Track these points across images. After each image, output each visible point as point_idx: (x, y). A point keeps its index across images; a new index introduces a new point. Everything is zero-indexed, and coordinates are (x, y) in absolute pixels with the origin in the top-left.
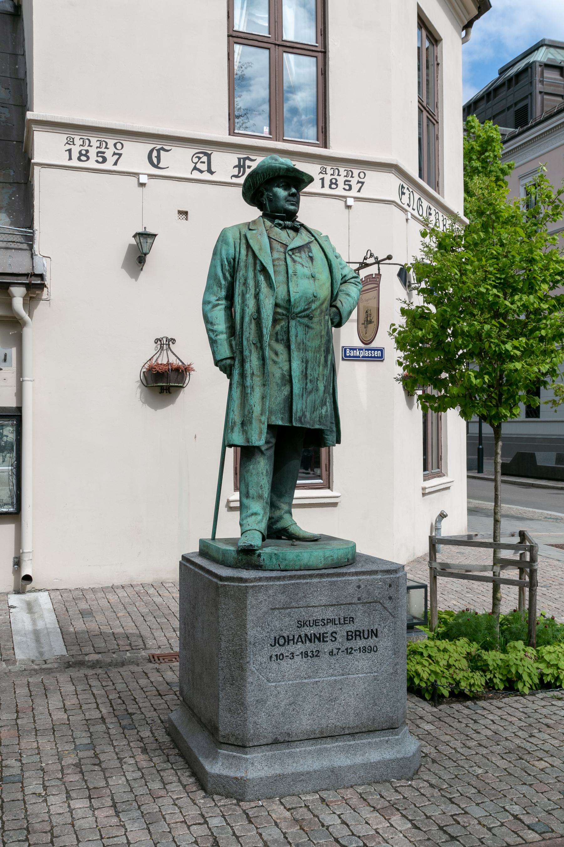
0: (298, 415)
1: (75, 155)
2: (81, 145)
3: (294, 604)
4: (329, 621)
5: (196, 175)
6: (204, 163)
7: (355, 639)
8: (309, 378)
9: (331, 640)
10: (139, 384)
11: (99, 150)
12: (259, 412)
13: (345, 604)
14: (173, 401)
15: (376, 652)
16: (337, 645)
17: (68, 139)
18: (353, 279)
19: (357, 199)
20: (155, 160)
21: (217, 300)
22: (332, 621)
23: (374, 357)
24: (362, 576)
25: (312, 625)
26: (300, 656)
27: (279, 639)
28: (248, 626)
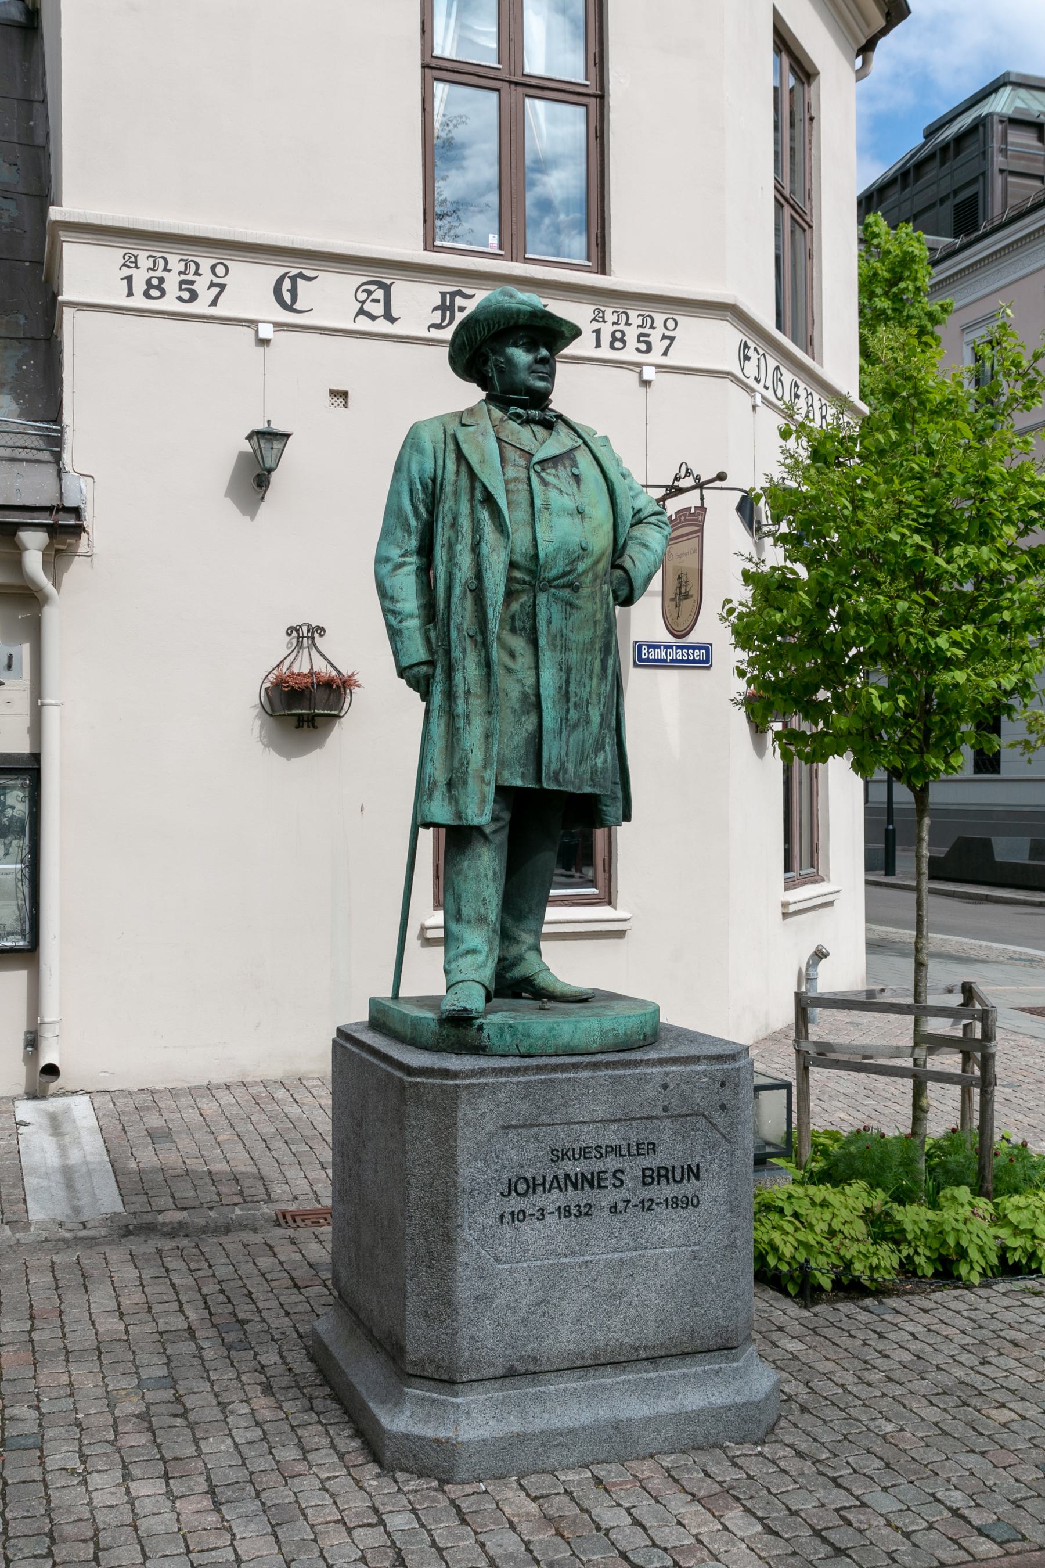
0: (552, 769)
1: (139, 287)
2: (149, 269)
3: (544, 1118)
4: (609, 1149)
5: (364, 324)
6: (378, 301)
7: (659, 1184)
8: (573, 699)
9: (614, 1185)
10: (258, 710)
11: (183, 277)
12: (481, 763)
13: (639, 1118)
14: (320, 743)
15: (696, 1206)
16: (624, 1193)
17: (127, 258)
18: (655, 517)
19: (661, 368)
20: (287, 297)
21: (403, 556)
22: (616, 1150)
23: (694, 661)
24: (671, 1066)
25: (577, 1156)
26: (557, 1214)
27: (516, 1182)
28: (460, 1160)
